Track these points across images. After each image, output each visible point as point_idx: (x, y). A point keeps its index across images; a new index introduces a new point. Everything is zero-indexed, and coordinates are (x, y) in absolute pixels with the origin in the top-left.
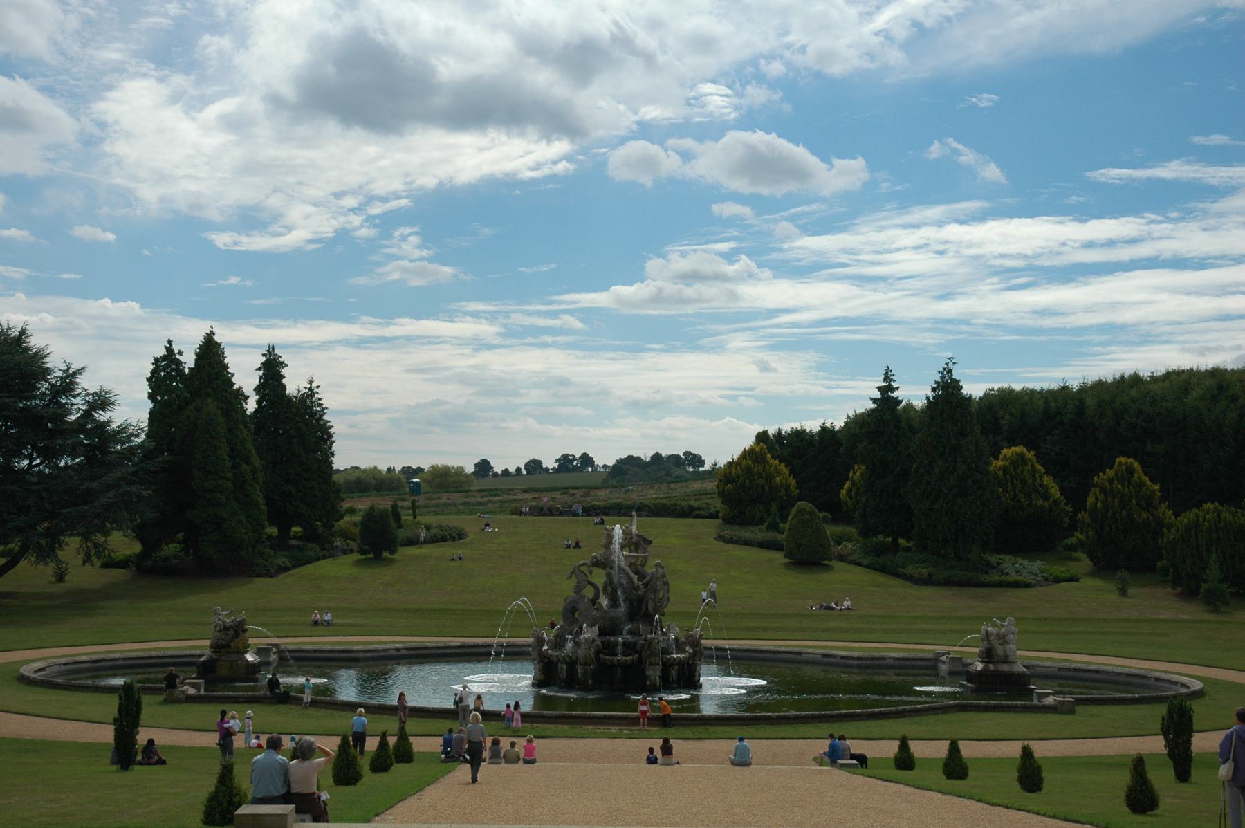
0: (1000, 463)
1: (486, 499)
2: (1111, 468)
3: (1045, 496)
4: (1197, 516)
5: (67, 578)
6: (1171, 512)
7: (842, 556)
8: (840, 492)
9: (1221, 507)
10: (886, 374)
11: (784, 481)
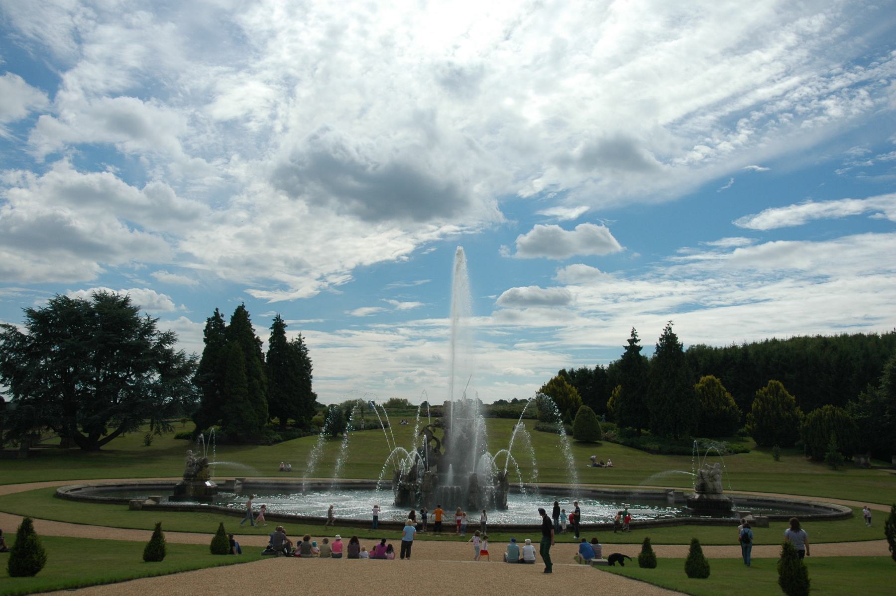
0: (700, 385)
1: (408, 410)
2: (766, 386)
3: (727, 404)
4: (820, 413)
5: (152, 444)
6: (802, 412)
7: (608, 438)
8: (606, 403)
9: (834, 407)
10: (633, 332)
11: (574, 397)
